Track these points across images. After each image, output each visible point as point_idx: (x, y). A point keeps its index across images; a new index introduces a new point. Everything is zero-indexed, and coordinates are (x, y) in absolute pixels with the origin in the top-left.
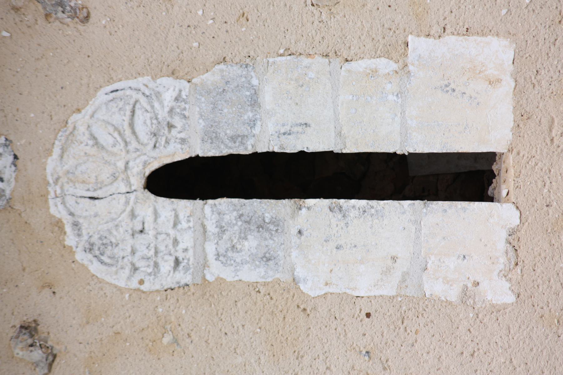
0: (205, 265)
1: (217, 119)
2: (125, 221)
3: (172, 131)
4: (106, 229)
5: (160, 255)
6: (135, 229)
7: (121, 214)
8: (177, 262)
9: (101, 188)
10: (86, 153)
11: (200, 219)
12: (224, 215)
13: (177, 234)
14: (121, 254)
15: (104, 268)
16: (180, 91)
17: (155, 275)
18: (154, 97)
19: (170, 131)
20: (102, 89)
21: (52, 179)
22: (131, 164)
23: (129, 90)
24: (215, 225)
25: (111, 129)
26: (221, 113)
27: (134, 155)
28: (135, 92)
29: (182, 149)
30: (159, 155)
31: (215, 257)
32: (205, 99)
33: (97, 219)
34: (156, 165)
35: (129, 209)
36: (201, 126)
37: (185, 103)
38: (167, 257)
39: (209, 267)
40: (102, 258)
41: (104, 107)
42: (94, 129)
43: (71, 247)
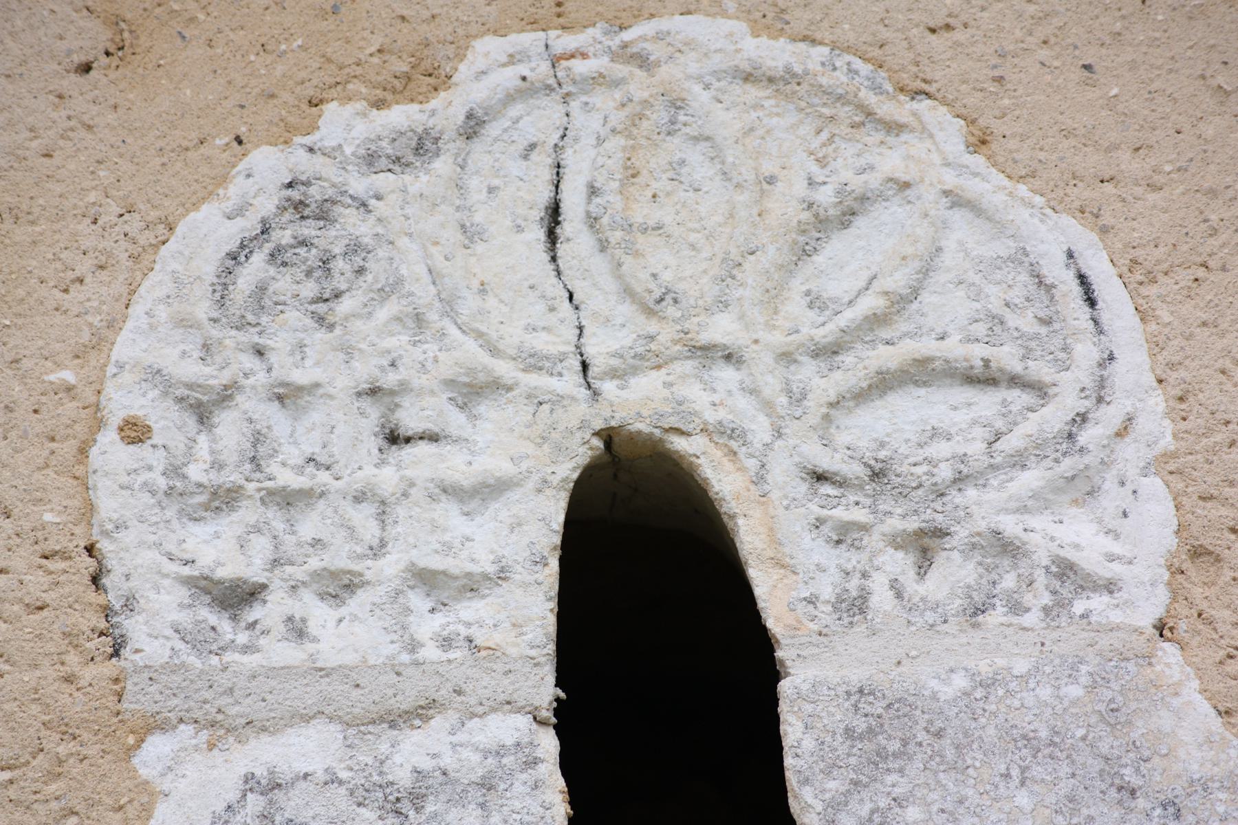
0: (220, 729)
1: (974, 757)
2: (442, 356)
3: (900, 555)
4: (404, 271)
5: (275, 518)
6: (406, 401)
7: (480, 335)
8: (237, 597)
9: (603, 246)
10: (771, 180)
11: (459, 692)
12: (482, 806)
13: (381, 590)
14: (279, 343)
15: (208, 267)
16: (1110, 587)
17: (169, 492)
18: (1068, 465)
19: (898, 542)
20: (1094, 237)
21: (643, 38)
22: (727, 375)
23: (1096, 355)
24: (426, 764)
25: (898, 281)
26: (1007, 776)
27: (771, 385)
28: (1088, 382)
29: (811, 601)
30: (775, 495)
31: (260, 772)
32: (1074, 703)
33: (451, 235)
34: (725, 482)
35: (504, 369)
36: (934, 684)
37: (1046, 610)
38: (261, 547)
39: (211, 746)
40: (258, 259)
41: (1003, 248)
42: (891, 213)
43: (312, 128)
